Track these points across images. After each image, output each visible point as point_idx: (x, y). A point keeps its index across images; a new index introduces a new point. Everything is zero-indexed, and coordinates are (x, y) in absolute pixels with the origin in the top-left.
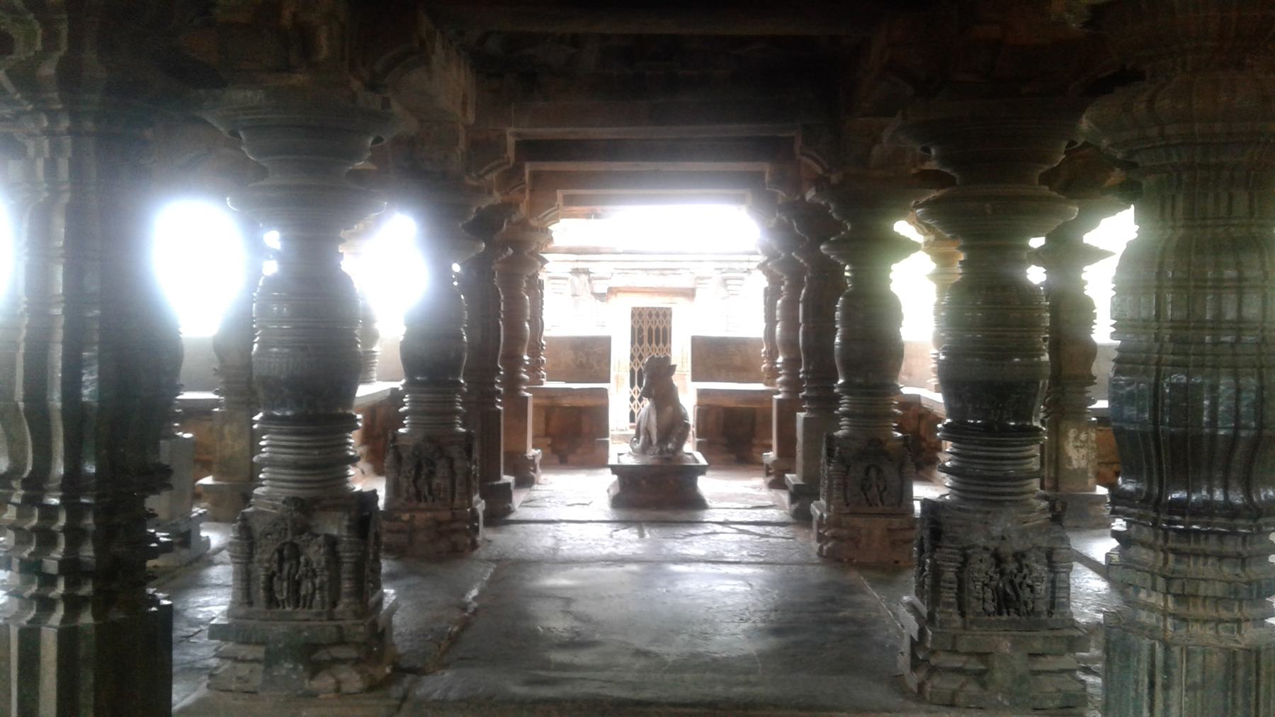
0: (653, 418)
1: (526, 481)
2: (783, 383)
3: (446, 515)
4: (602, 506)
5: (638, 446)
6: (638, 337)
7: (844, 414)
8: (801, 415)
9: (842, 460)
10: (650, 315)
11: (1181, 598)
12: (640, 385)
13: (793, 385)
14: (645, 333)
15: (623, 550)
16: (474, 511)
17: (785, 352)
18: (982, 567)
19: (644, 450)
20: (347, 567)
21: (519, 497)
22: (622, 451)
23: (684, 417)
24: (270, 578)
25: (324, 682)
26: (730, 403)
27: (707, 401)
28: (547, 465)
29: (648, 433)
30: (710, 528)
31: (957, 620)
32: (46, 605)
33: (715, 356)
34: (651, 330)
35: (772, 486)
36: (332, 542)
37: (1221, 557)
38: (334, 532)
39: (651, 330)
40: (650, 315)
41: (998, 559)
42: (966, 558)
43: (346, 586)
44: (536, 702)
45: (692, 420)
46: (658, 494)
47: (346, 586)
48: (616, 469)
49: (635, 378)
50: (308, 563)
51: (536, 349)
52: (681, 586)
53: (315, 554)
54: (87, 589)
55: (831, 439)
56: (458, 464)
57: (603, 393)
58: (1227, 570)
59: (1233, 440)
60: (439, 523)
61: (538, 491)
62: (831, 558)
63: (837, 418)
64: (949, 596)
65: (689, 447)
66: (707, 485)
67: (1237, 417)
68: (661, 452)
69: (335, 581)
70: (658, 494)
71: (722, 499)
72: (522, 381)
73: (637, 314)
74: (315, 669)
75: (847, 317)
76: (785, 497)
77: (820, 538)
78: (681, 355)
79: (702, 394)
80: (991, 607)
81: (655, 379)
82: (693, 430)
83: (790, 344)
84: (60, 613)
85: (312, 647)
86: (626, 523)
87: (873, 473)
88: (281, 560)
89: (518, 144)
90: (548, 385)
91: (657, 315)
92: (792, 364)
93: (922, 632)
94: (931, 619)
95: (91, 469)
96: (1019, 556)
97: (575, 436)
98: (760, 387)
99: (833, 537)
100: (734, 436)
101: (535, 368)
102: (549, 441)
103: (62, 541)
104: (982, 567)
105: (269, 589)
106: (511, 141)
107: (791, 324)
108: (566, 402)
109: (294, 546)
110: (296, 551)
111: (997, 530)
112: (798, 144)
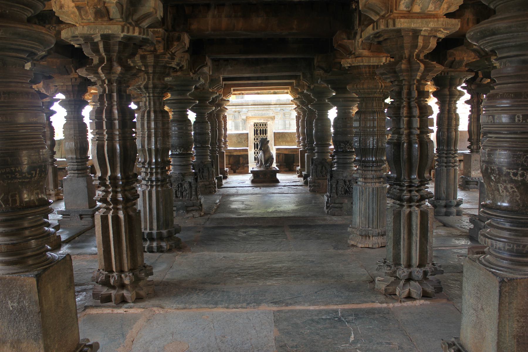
0: (263, 156)
1: (225, 178)
2: (302, 145)
3: (207, 183)
4: (248, 183)
5: (258, 165)
6: (256, 132)
7: (316, 152)
8: (306, 154)
9: (316, 165)
10: (260, 125)
11: (365, 178)
12: (257, 148)
13: (304, 146)
14: (259, 131)
15: (257, 192)
16: (215, 182)
17: (302, 136)
18: (341, 183)
19: (260, 167)
20: (193, 188)
21: (224, 181)
22: (253, 166)
23: (272, 156)
24: (176, 192)
25: (190, 215)
26: (286, 152)
27: (278, 152)
28: (230, 173)
29: (261, 161)
30: (280, 187)
31: (336, 196)
32: (152, 186)
33: (279, 137)
34: (261, 130)
35: (299, 176)
36: (190, 183)
37: (372, 171)
38: (190, 180)
39: (261, 130)
40: (260, 125)
41: (345, 182)
42: (338, 182)
43: (194, 193)
44: (239, 218)
45: (275, 157)
46: (265, 178)
47: (194, 193)
48: (252, 172)
49: (256, 146)
50: (185, 188)
51: (225, 136)
52: (272, 198)
53: (186, 186)
54: (159, 183)
55: (312, 159)
56: (210, 169)
57: (246, 150)
58: (373, 173)
59: (373, 148)
60: (206, 185)
61: (228, 180)
62: (312, 191)
63: (314, 153)
64: (334, 191)
65: (274, 165)
66: (279, 176)
67: (373, 144)
68: (265, 166)
69: (191, 192)
70: (265, 178)
71: (284, 180)
72: (222, 147)
73: (256, 125)
74: (188, 212)
75: (316, 125)
76: (302, 179)
77: (310, 186)
78: (270, 136)
79: (277, 149)
80: (343, 193)
81: (262, 145)
82: (275, 161)
83: (303, 133)
84: (154, 188)
85: (187, 207)
86: (256, 187)
87: (324, 168)
88: (179, 187)
89: (223, 78)
90: (229, 148)
91: (263, 125)
92: (304, 139)
93: (328, 199)
94: (330, 197)
95: (159, 160)
96: (350, 181)
97: (239, 164)
98: (296, 147)
99: (313, 186)
100: (288, 162)
101: (225, 144)
102: (230, 166)
103: (154, 174)
104: (341, 183)
105: (176, 194)
106: (221, 78)
107: (303, 128)
108: (235, 154)
109: (181, 184)
110: (182, 185)
111: (345, 175)
112: (301, 78)
